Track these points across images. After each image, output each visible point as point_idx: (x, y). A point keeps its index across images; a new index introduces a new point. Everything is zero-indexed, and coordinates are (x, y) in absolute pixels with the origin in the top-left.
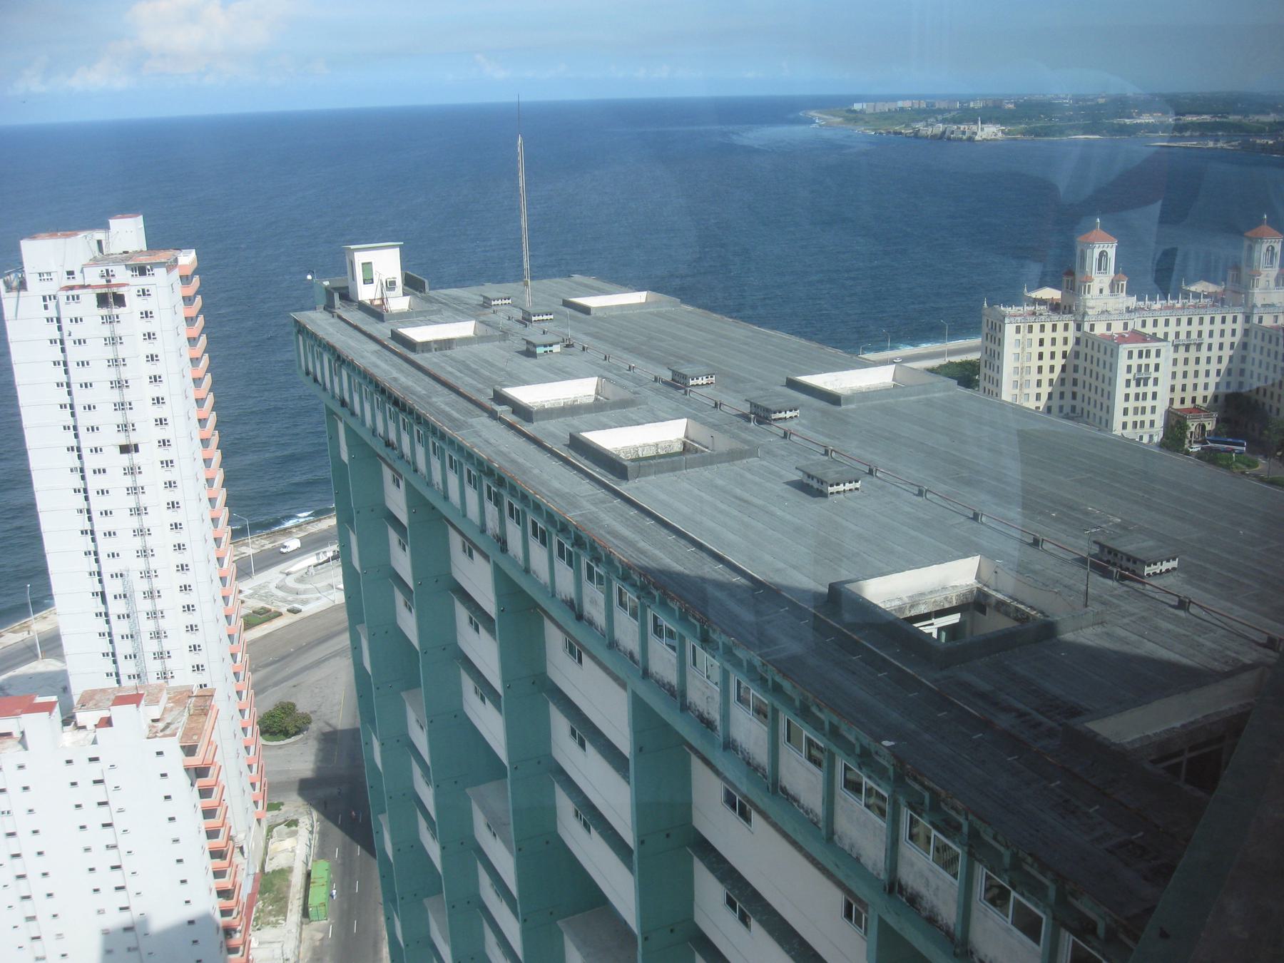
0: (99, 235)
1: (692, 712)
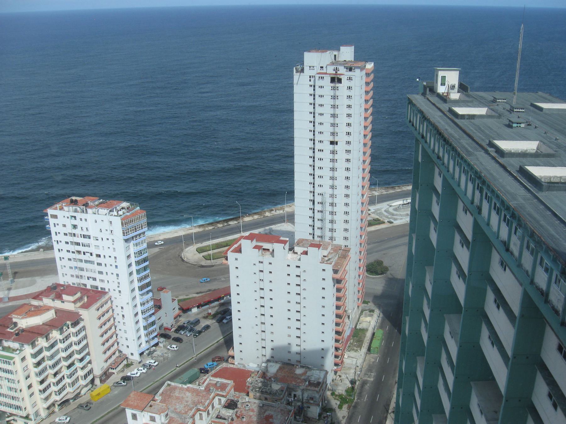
0: (336, 53)
1: (550, 304)
